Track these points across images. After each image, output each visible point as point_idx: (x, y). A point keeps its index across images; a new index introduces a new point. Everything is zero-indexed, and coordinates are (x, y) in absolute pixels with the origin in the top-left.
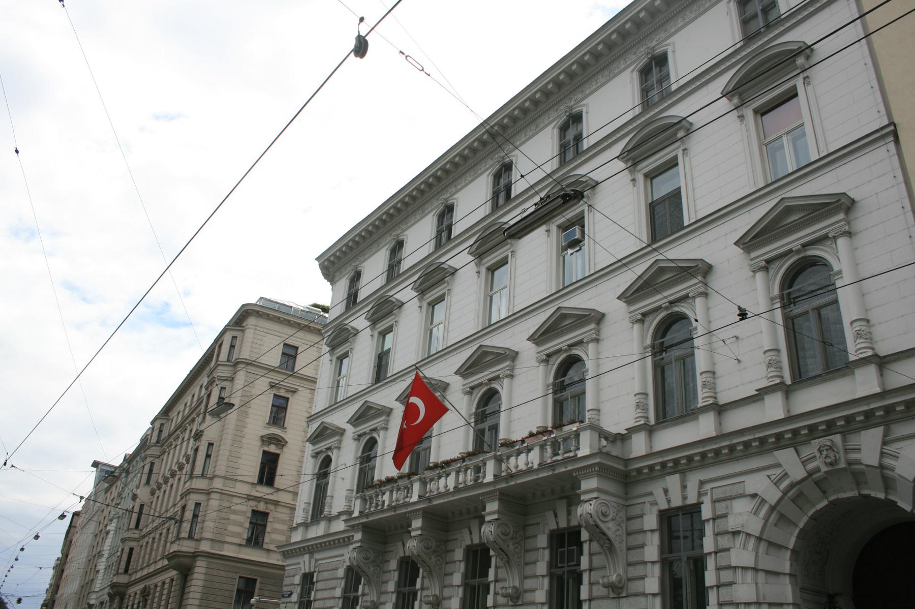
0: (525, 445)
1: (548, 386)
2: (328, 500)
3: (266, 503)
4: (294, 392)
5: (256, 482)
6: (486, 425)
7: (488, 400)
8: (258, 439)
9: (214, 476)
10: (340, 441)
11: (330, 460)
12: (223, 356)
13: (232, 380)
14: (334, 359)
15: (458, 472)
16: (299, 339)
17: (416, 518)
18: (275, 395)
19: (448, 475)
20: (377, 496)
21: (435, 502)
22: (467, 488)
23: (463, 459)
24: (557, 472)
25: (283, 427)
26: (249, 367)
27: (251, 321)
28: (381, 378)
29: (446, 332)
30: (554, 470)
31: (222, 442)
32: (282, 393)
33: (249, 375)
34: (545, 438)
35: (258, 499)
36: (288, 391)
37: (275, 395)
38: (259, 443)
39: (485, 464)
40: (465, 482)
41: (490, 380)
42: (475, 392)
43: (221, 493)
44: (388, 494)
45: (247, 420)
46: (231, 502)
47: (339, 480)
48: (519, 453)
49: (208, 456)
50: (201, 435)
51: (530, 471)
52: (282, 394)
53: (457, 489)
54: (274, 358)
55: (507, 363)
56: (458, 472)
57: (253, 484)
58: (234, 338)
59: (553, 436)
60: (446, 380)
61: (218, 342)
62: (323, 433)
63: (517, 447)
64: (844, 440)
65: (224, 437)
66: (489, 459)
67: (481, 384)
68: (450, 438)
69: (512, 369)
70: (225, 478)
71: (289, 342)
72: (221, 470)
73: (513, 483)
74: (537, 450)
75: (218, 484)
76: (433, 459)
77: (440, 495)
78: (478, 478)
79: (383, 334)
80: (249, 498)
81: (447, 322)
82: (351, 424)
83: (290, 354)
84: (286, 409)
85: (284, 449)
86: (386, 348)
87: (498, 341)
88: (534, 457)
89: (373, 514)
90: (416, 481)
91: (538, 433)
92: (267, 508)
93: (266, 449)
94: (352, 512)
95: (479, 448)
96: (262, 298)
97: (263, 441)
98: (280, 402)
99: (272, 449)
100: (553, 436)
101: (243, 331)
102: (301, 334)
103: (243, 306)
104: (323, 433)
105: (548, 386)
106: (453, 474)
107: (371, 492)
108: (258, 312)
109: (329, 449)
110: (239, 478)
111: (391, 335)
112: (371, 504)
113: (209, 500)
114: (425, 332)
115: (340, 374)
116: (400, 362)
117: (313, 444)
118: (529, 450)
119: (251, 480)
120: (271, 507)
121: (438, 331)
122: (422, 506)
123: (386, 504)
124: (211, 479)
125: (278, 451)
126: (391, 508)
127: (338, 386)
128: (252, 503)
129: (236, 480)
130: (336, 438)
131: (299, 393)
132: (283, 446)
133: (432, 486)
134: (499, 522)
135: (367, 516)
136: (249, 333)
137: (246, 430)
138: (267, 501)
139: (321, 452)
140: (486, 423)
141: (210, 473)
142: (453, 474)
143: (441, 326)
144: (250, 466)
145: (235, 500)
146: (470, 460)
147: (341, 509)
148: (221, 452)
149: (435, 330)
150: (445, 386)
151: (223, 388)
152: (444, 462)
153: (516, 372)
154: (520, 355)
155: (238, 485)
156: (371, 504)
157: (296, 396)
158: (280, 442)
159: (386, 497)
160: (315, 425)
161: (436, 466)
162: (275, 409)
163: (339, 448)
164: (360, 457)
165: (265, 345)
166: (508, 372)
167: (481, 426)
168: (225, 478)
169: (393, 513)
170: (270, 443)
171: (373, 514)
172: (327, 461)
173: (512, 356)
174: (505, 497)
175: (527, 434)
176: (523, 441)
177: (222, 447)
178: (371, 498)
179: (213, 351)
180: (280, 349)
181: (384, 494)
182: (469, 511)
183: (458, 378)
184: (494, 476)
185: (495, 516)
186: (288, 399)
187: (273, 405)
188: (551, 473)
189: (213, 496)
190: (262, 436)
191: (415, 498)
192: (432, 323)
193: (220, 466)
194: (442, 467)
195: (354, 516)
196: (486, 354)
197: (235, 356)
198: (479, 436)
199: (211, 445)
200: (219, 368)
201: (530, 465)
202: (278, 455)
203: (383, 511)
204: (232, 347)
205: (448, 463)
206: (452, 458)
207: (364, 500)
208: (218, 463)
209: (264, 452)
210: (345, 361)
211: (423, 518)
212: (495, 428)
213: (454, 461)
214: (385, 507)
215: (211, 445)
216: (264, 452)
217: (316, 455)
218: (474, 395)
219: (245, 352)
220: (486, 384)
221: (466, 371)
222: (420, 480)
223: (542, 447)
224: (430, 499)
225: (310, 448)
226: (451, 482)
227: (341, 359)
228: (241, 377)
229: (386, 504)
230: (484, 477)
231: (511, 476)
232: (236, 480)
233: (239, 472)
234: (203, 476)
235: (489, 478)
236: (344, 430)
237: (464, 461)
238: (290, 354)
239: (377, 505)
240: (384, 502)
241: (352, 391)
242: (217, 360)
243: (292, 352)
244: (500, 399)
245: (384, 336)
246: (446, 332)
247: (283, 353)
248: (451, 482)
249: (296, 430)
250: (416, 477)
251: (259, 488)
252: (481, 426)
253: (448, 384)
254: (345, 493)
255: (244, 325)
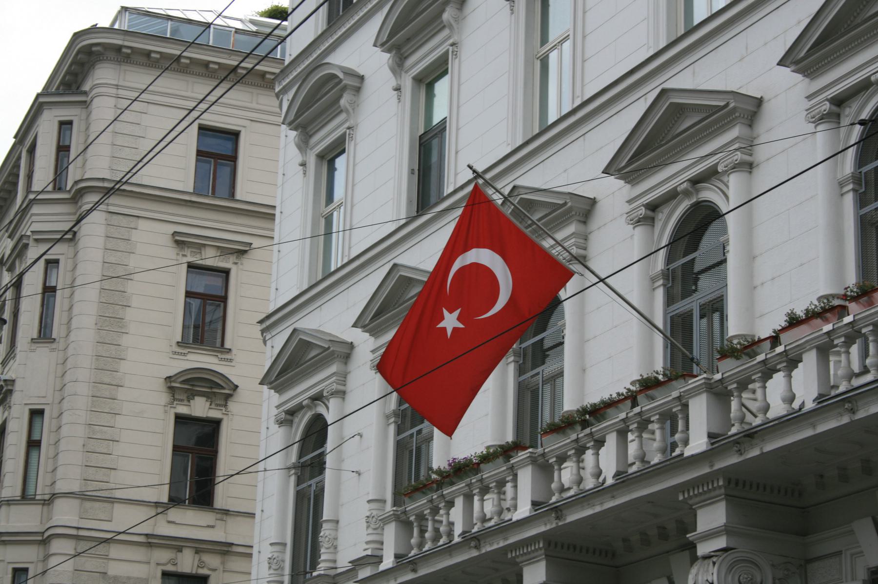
0: (780, 349)
1: (841, 185)
2: (326, 531)
3: (198, 551)
4: (241, 253)
5: (165, 499)
6: (693, 304)
7: (692, 237)
8: (160, 385)
9: (54, 496)
10: (343, 377)
11: (325, 426)
12: (43, 174)
13: (70, 236)
14: (312, 160)
15: (622, 434)
16: (232, 109)
17: (531, 561)
18: (191, 266)
19: (600, 443)
20: (435, 511)
21: (572, 517)
22: (650, 473)
23: (632, 398)
24: (861, 414)
25: (221, 349)
26: (113, 200)
27: (104, 75)
28: (433, 200)
29: (579, 61)
30: (853, 411)
31: (66, 405)
32: (210, 258)
33: (116, 219)
34: (828, 327)
35: (177, 544)
36: (225, 252)
37: (191, 266)
38: (164, 397)
39: (686, 406)
40: (642, 458)
41: (696, 181)
42: (661, 216)
43: (77, 538)
44: (459, 502)
45: (125, 340)
46: (106, 557)
47: (348, 478)
48: (768, 372)
49: (33, 444)
50: (10, 392)
51: (796, 418)
52: (209, 263)
53: (623, 480)
54: (176, 169)
55: (734, 132)
56: (622, 434)
57: (157, 504)
58: (65, 125)
59: (848, 319)
60: (587, 191)
61: (25, 135)
62: (298, 360)
63: (761, 357)
64: (223, 563)
65: (68, 389)
66: (695, 392)
67: (672, 196)
68: (607, 340)
69: (749, 145)
70: (82, 496)
71: (212, 119)
72: (69, 479)
73: (755, 452)
74: (810, 359)
75: (65, 514)
76: (570, 404)
77: (584, 498)
78: (674, 446)
79: (427, 82)
80: (152, 541)
81: (578, 34)
82: (364, 328)
83: (219, 151)
84: (224, 299)
85: (232, 405)
86: (436, 120)
87: (709, 74)
88: (805, 384)
89: (426, 558)
90: (522, 464)
91: (812, 316)
92: (202, 564)
93: (183, 410)
94: (379, 559)
95: (681, 364)
96: (124, 9)
97: (171, 389)
98: (202, 284)
99: (200, 408)
100: (848, 319)
101: (85, 105)
102: (239, 96)
103: (77, 36)
104: (298, 360)
105: (841, 185)
106: (612, 440)
107: (420, 503)
108: (118, 49)
109: (318, 398)
110: (118, 494)
111: (446, 80)
112: (422, 532)
113: (47, 557)
114: (528, 64)
115: (330, 198)
116: (471, 152)
117: (279, 389)
118: (792, 362)
119: (151, 495)
120: (212, 561)
121: (559, 62)
122: (542, 529)
123: (458, 530)
124: (49, 502)
125: (214, 414)
126: (471, 539)
127: (328, 233)
128: (163, 556)
129: (112, 500)
130: (333, 369)
131: (253, 254)
132: (228, 397)
133: (567, 474)
134: (731, 556)
135: (413, 565)
136: (103, 109)
137: (124, 367)
138: (200, 547)
139: (299, 408)
140: (695, 296)
141: (41, 490)
142: (612, 440)
143: (567, 45)
144: (146, 458)
145: (115, 551)
146: (652, 398)
147: (359, 552)
148: (65, 431)
149: (553, 57)
150: (584, 209)
151: (51, 264)
152: (584, 411)
153: (761, 153)
154: (767, 107)
155: (119, 510)
156: (422, 532)
157: (247, 263)
158: (218, 388)
159: (457, 514)
160: (279, 339)
161: (567, 424)
162: (195, 303)
163: (341, 394)
164: (395, 414)
165: (145, 132)
166: (739, 156)
167: (681, 306)
168: (82, 496)
169: (474, 553)
170: (191, 395)
171: (426, 558)
172: (316, 433)
173: (749, 110)
174: (740, 488)
175: (781, 321)
176: (775, 340)
177: (65, 418)
178: (421, 518)
179: (17, 166)
180: (190, 141)
181: (450, 504)
182: (663, 534)
183: (614, 183)
184: (711, 436)
185: (721, 543)
186: (226, 272)
187: (189, 294)
188: (845, 420)
189: (57, 546)
190: (168, 379)
191: (524, 510)
192: (544, 39)
193: (66, 467)
194: (585, 424)
195: (383, 567)
196: (678, 111)
197: (73, 174)
198: (679, 330)
199: (36, 414)
200: (35, 209)
201: (796, 405)
202: (216, 424)
203: (451, 549)
204: (63, 149)
205: (598, 412)
206: (606, 396)
207: (404, 523)
208: (61, 459)
209: (180, 420)
210: (340, 162)
211: (548, 557)
212: (716, 307)
213: (610, 404)
214: (457, 539)
215: (36, 414)
216: (180, 420)
217: (289, 417)
218: (658, 225)
219: (98, 164)
220: (687, 194)
221: (631, 163)
222: (533, 460)
223: (824, 350)
224: (558, 511)
225: (270, 402)
226: (608, 460)
227: (329, 157)
228: (94, 228)
229: (458, 530)
230: (686, 442)
231: (751, 435)
232: (112, 500)
233: (116, 478)
234: (25, 497)
235: (698, 443)
236: (351, 346)
237: (635, 404)
238: (219, 151)
239: (437, 536)
240: (451, 524)
241: (361, 241)
242: (28, 190)
243: (221, 146)
244: (724, 230)
245: (430, 87)
246: (579, 61)
247: (199, 153)
248: (608, 460)
249: (248, 356)
250: (523, 455)
251: (175, 514)
252: (681, 306)
253: (593, 202)
254: (365, 510)
255: (86, 87)
